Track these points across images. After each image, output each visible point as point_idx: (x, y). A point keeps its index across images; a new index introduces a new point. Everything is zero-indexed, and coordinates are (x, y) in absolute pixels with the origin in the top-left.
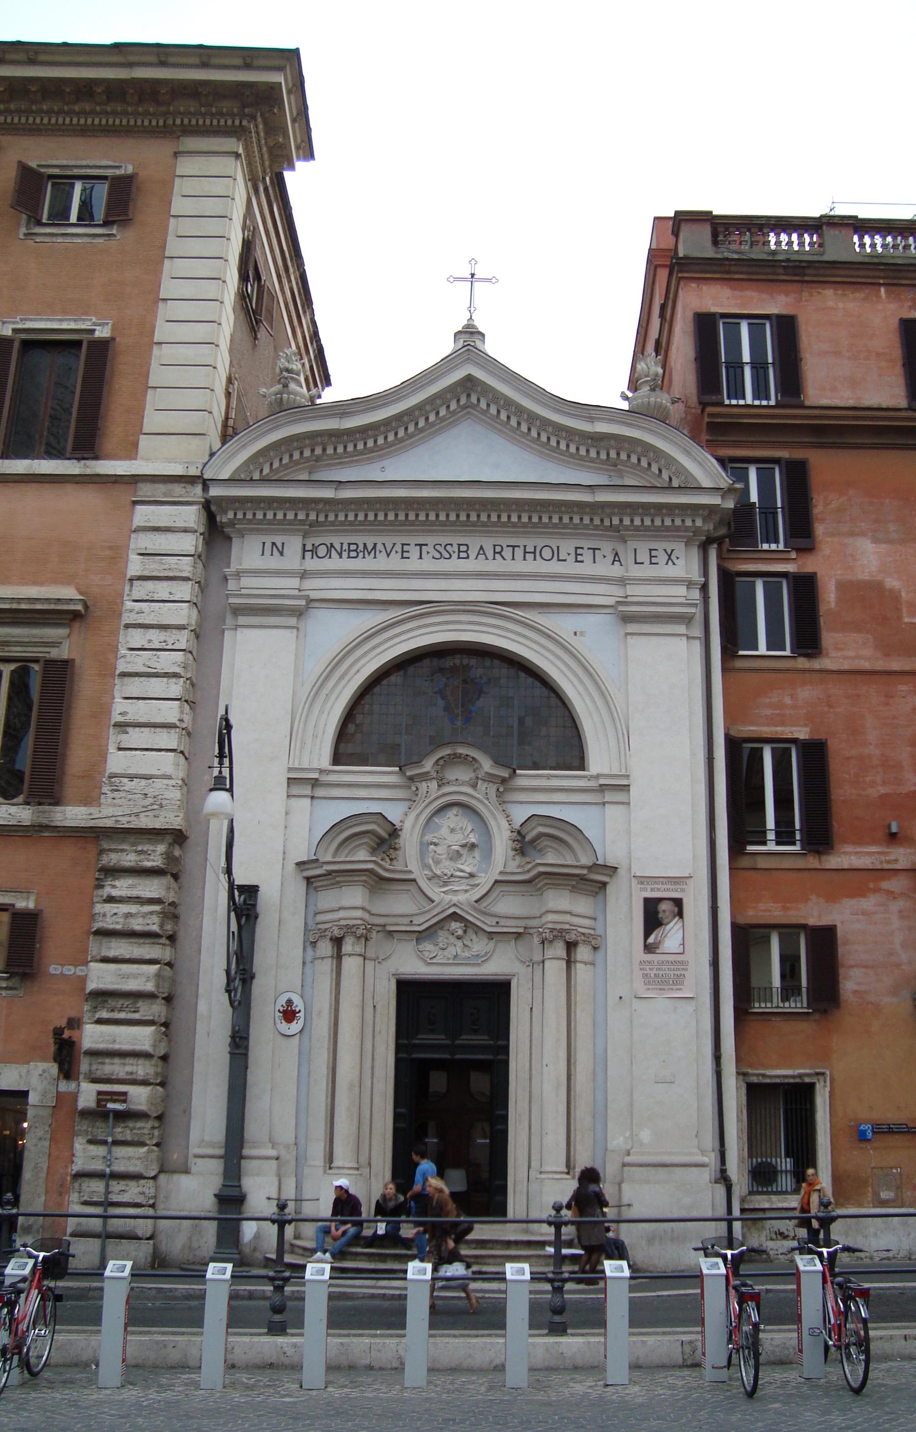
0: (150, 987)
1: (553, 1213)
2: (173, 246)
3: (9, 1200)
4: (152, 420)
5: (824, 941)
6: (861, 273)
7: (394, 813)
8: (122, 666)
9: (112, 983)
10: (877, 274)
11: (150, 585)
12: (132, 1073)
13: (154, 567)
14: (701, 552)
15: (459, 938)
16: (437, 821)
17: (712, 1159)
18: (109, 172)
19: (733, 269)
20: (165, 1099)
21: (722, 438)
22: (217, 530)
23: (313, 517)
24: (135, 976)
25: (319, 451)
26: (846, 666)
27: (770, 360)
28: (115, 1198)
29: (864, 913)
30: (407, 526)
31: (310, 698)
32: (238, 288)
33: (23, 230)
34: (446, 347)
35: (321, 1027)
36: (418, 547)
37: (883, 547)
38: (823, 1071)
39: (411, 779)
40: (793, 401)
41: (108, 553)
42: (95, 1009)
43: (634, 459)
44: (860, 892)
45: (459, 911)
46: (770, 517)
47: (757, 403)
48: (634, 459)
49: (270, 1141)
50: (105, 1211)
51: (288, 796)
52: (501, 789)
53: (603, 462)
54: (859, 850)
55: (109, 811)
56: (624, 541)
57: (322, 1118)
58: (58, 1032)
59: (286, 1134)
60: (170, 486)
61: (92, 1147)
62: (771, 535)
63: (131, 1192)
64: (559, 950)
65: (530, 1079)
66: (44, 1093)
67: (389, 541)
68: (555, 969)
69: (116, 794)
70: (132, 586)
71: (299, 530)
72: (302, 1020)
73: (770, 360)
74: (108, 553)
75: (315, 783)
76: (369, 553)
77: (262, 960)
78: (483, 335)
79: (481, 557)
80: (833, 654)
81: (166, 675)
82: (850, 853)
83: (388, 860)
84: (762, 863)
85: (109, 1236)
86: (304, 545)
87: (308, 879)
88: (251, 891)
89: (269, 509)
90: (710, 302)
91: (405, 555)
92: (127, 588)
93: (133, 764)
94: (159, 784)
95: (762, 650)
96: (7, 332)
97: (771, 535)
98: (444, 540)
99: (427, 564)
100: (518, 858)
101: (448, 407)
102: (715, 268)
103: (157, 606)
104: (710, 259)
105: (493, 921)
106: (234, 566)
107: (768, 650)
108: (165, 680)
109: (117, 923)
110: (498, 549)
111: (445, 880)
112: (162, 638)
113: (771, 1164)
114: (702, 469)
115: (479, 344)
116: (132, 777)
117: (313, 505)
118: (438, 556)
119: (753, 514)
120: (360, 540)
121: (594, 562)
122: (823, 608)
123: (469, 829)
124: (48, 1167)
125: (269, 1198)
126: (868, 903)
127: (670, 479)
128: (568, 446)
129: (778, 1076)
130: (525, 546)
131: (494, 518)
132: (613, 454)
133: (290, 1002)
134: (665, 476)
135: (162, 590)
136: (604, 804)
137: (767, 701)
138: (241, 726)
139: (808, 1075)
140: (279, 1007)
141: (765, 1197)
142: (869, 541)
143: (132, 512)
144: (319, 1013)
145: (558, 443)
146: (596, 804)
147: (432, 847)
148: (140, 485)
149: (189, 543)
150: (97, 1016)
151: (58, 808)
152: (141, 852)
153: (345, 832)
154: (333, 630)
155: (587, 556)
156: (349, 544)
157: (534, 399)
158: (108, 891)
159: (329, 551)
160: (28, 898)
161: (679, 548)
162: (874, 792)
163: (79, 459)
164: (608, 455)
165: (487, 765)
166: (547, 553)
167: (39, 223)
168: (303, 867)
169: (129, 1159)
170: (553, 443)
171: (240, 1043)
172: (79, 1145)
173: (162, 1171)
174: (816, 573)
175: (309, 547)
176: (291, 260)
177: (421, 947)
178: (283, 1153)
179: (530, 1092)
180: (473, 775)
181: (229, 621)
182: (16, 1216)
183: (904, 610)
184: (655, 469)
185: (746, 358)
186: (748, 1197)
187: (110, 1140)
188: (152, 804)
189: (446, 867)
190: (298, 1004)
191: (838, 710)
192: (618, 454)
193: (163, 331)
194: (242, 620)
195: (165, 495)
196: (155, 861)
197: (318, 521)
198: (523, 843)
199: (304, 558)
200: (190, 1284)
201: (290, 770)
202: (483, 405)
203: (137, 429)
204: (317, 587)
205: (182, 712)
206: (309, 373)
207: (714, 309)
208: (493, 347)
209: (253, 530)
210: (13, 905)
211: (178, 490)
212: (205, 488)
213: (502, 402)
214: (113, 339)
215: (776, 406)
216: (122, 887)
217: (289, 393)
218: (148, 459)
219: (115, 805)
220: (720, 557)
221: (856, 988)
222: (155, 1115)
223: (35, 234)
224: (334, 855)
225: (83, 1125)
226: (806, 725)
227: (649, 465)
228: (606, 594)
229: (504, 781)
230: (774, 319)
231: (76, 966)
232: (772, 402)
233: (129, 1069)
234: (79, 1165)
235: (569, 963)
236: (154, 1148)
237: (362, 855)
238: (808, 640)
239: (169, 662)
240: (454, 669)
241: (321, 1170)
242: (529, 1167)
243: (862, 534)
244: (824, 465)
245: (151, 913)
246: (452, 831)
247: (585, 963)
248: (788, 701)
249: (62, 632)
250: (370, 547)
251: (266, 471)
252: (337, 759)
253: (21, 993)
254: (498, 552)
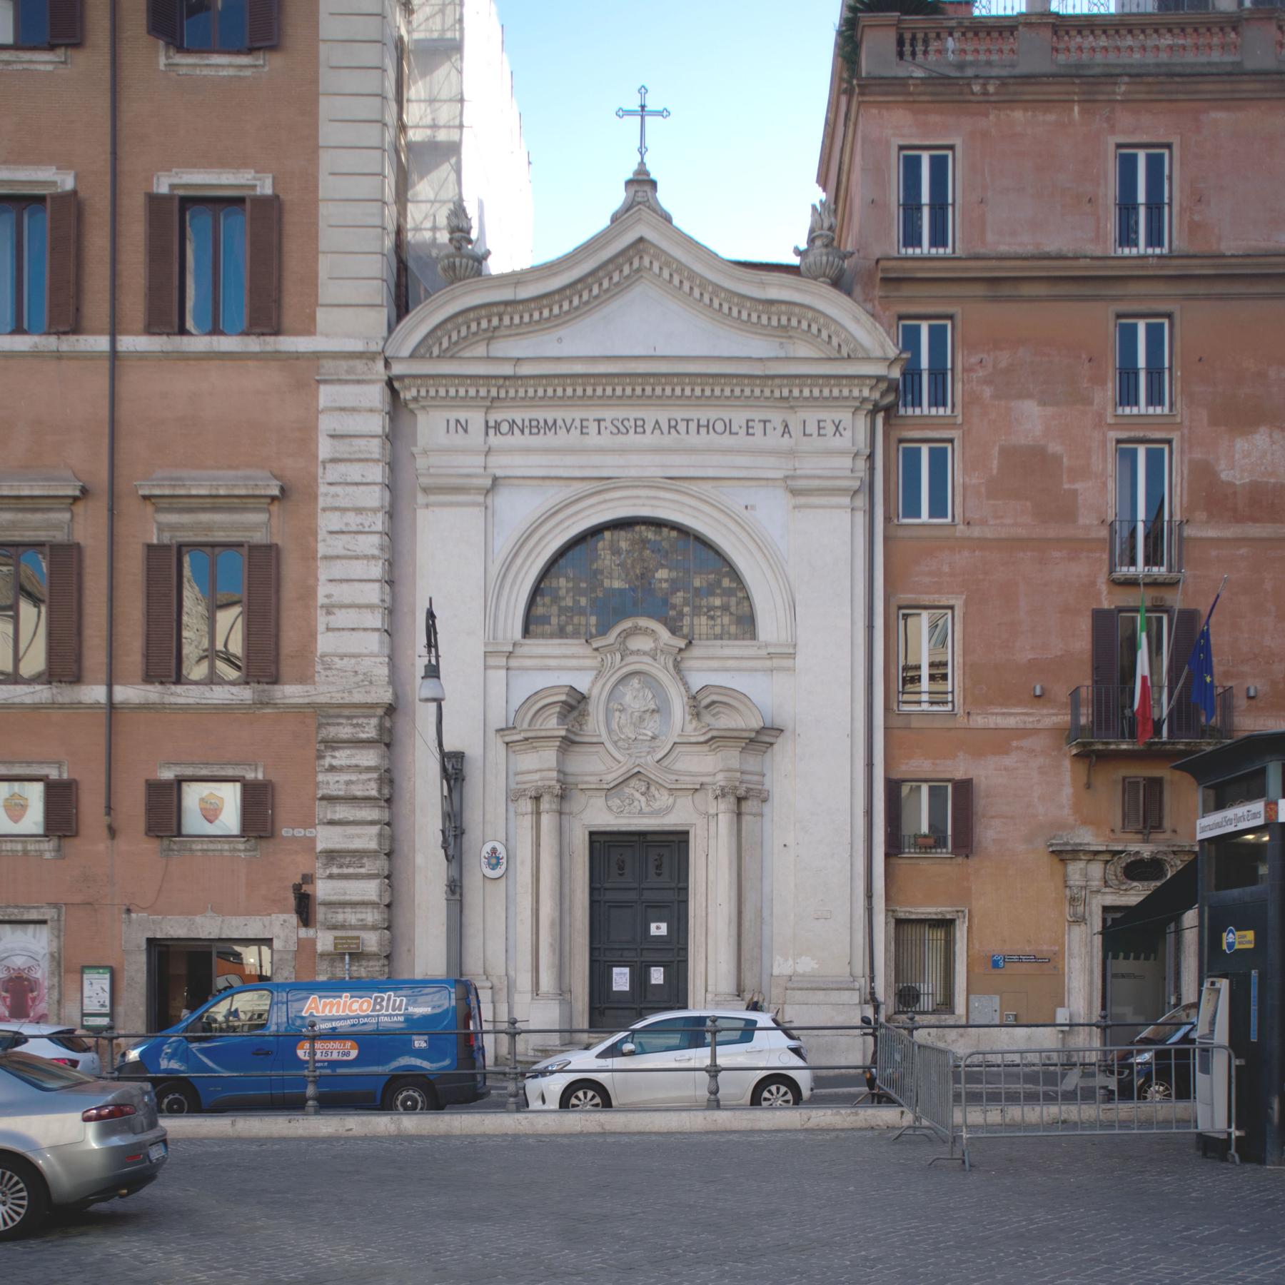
0: (373, 845)
2: (327, 79)
4: (329, 291)
8: (322, 550)
11: (342, 468)
13: (343, 448)
14: (869, 419)
17: (862, 982)
20: (392, 941)
23: (494, 392)
25: (495, 322)
33: (162, 61)
34: (617, 197)
37: (1050, 410)
43: (804, 325)
48: (804, 325)
55: (324, 690)
59: (498, 968)
60: (351, 363)
69: (328, 673)
77: (473, 818)
79: (657, 432)
81: (366, 557)
86: (487, 422)
88: (459, 757)
92: (320, 470)
93: (343, 645)
94: (367, 662)
95: (925, 516)
100: (694, 722)
116: (342, 657)
118: (615, 431)
126: (1009, 761)
131: (668, 391)
144: (523, 863)
151: (276, 687)
152: (357, 725)
159: (511, 428)
161: (845, 416)
171: (455, 888)
175: (492, 423)
183: (1065, 476)
194: (432, 498)
195: (348, 372)
199: (487, 434)
203: (312, 302)
204: (501, 464)
205: (383, 593)
216: (342, 757)
218: (327, 336)
219: (329, 683)
223: (177, 65)
226: (962, 593)
227: (819, 330)
233: (360, 916)
241: (529, 996)
243: (1030, 396)
250: (550, 423)
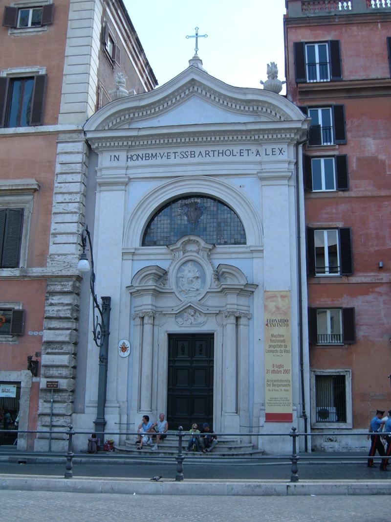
0: (67, 339)
1: (292, 431)
2: (70, 33)
3: (181, 429)
4: (64, 108)
5: (349, 315)
6: (369, 18)
7: (164, 265)
8: (54, 210)
9: (53, 338)
10: (376, 17)
11: (64, 176)
12: (61, 374)
13: (65, 168)
15: (192, 316)
16: (183, 267)
18: (43, 4)
19: (311, 21)
21: (306, 98)
22: (91, 151)
23: (130, 143)
24: (61, 335)
25: (132, 116)
26: (360, 194)
27: (328, 61)
28: (55, 424)
29: (367, 302)
30: (168, 145)
32: (101, 48)
35: (137, 354)
36: (247, 151)
37: (378, 141)
38: (348, 370)
39: (172, 250)
40: (337, 78)
41: (48, 164)
42: (46, 349)
43: (264, 110)
44: (366, 293)
45: (192, 305)
46: (328, 131)
47: (322, 81)
48: (264, 110)
49: (117, 401)
50: (51, 430)
51: (122, 259)
52: (209, 254)
53: (251, 112)
54: (365, 274)
55: (50, 270)
56: (260, 145)
57: (136, 390)
58: (30, 358)
60: (71, 135)
61: (45, 404)
62: (328, 139)
63: (61, 421)
64: (232, 320)
65: (222, 374)
66: (27, 382)
67: (162, 151)
68: (230, 328)
69: (53, 262)
70: (57, 177)
71: (125, 149)
72: (129, 352)
73: (328, 61)
74: (48, 164)
75: (133, 254)
76: (154, 157)
78: (201, 61)
80: (354, 190)
81: (72, 213)
82: (361, 276)
83: (162, 284)
84: (322, 281)
85: (52, 439)
87: (131, 293)
88: (107, 300)
89: (112, 142)
90: (300, 37)
91: (169, 157)
92: (55, 178)
94: (70, 257)
96: (4, 75)
97: (328, 139)
98: (184, 150)
99: (178, 161)
100: (216, 282)
101: (185, 93)
102: (303, 22)
103: (67, 186)
104: (301, 18)
105: (170, 309)
106: (99, 166)
107: (326, 189)
108: (71, 215)
109: (54, 314)
110: (207, 152)
111: (187, 292)
112: (70, 198)
113: (326, 410)
114: (293, 112)
115: (200, 66)
116: (59, 255)
117: (129, 139)
119: (320, 130)
120: (150, 152)
121: (248, 155)
122: (350, 170)
123: (196, 270)
124: (29, 411)
125: (116, 423)
126: (370, 298)
127: (280, 117)
128: (236, 106)
129: (329, 372)
130: (219, 151)
132: (255, 108)
133: (124, 343)
134: (278, 116)
135: (69, 178)
136: (253, 258)
137: (325, 211)
138: (102, 232)
139: (342, 372)
140: (120, 346)
141: (323, 424)
142: (371, 139)
143: (56, 147)
145: (232, 105)
146: (250, 258)
147: (181, 279)
148: (60, 135)
149: (79, 158)
150: (47, 351)
153: (142, 274)
154: (139, 190)
155: (245, 153)
156: (146, 154)
157: (221, 87)
158: (50, 301)
160: (19, 305)
161: (284, 147)
162: (372, 249)
163: (34, 126)
164: (253, 108)
165: (203, 243)
166: (228, 153)
167: (15, 28)
168: (128, 288)
169: (59, 408)
170: (229, 105)
171: (104, 360)
172: (41, 401)
173: (74, 413)
174: (347, 155)
175: (129, 156)
176: (131, 33)
177: (177, 320)
178: (122, 404)
179: (222, 379)
180: (197, 248)
181: (98, 189)
182: (104, 434)
184: (273, 113)
185: (317, 61)
186: (316, 424)
187: (52, 400)
188: (67, 266)
189: (186, 287)
190: (127, 344)
191: (356, 214)
192: (257, 108)
193: (67, 69)
194: (103, 188)
196: (68, 288)
197: (130, 144)
198: (219, 275)
199: (127, 161)
200: (263, 463)
201: (123, 249)
202: (200, 91)
203: (58, 111)
204: (132, 173)
205: (78, 227)
206: (146, 80)
207: (302, 40)
208: (206, 67)
209: (106, 151)
210: (14, 308)
211: (75, 135)
212: (85, 133)
213: (207, 89)
214: (47, 75)
215: (331, 81)
216: (55, 299)
217: (120, 92)
218: (62, 124)
219: (52, 267)
220: (304, 149)
221: (363, 334)
222: (70, 390)
223: (14, 33)
224: (139, 284)
225: (42, 395)
226: (342, 221)
227: (271, 112)
228: (253, 169)
229: (210, 250)
230: (329, 43)
231: (38, 332)
232: (329, 80)
233: (59, 372)
234: (40, 411)
235: (237, 325)
236: (70, 404)
237: (151, 283)
238: (343, 184)
239: (73, 207)
240: (191, 204)
241: (136, 411)
242: (222, 410)
243: (369, 136)
244: (350, 105)
245: (67, 309)
246: (189, 271)
247: (245, 325)
248: (334, 211)
249: (30, 197)
251: (111, 125)
252: (143, 244)
253: (17, 343)
254: (207, 154)
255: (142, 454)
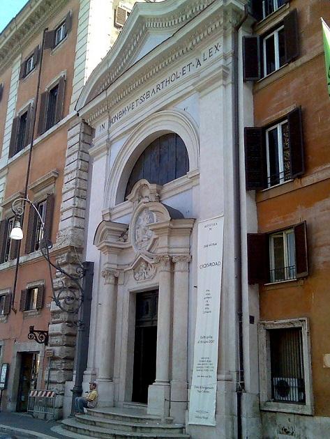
31: (174, 193)
129: (280, 324)
137: (275, 99)
248: (285, 93)
255: (138, 430)
